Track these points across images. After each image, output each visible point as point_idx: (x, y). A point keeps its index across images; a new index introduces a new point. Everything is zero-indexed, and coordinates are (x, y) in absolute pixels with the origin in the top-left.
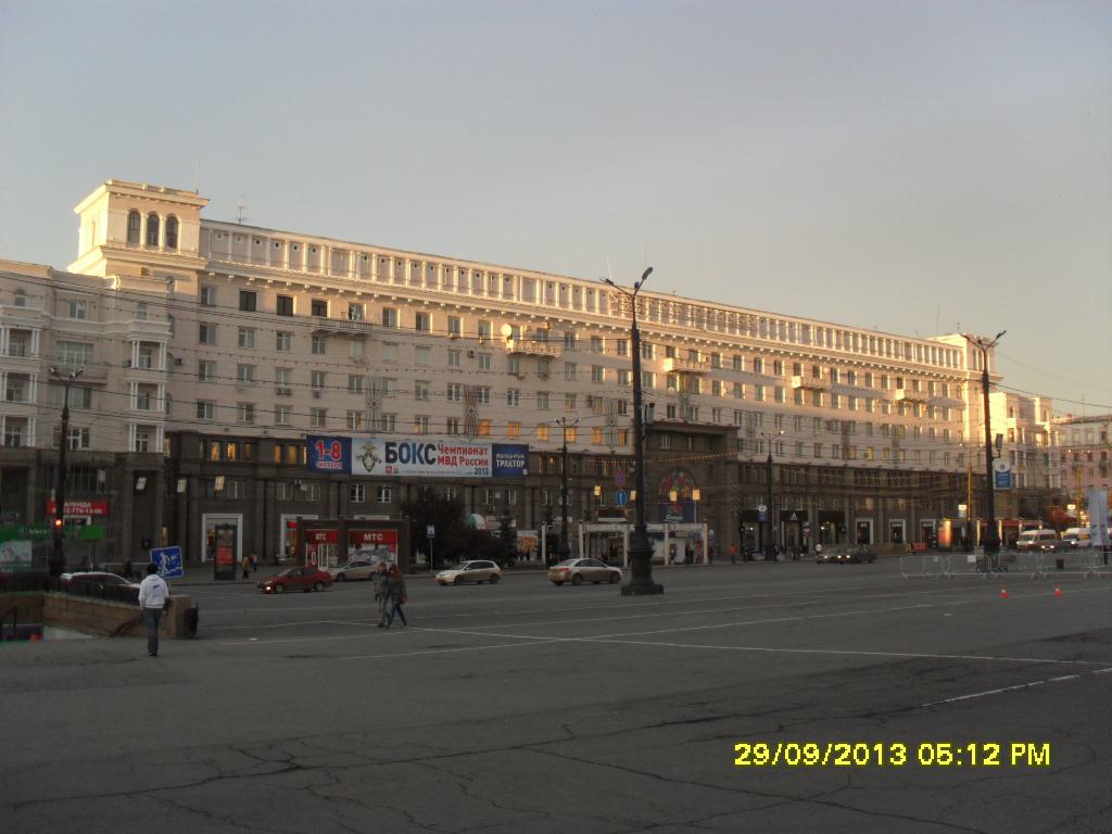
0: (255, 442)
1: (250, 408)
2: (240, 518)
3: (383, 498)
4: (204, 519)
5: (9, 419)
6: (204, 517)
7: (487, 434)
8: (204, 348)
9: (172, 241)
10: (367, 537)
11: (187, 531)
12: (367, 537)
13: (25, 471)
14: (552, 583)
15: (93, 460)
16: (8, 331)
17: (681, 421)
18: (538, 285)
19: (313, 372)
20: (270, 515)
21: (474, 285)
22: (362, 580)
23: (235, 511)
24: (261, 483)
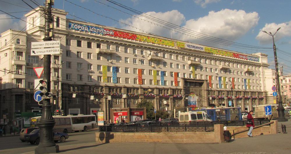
0: (83, 86)
1: (81, 76)
2: (79, 109)
3: (118, 104)
4: (77, 109)
5: (125, 57)
6: (69, 109)
7: (54, 97)
8: (68, 58)
10: (135, 113)
11: (157, 104)
12: (135, 113)
13: (22, 95)
14: (21, 141)
16: (16, 52)
17: (193, 79)
18: (60, 57)
19: (98, 65)
20: (88, 108)
21: (30, 60)
22: (77, 131)
23: (78, 108)
24: (85, 99)
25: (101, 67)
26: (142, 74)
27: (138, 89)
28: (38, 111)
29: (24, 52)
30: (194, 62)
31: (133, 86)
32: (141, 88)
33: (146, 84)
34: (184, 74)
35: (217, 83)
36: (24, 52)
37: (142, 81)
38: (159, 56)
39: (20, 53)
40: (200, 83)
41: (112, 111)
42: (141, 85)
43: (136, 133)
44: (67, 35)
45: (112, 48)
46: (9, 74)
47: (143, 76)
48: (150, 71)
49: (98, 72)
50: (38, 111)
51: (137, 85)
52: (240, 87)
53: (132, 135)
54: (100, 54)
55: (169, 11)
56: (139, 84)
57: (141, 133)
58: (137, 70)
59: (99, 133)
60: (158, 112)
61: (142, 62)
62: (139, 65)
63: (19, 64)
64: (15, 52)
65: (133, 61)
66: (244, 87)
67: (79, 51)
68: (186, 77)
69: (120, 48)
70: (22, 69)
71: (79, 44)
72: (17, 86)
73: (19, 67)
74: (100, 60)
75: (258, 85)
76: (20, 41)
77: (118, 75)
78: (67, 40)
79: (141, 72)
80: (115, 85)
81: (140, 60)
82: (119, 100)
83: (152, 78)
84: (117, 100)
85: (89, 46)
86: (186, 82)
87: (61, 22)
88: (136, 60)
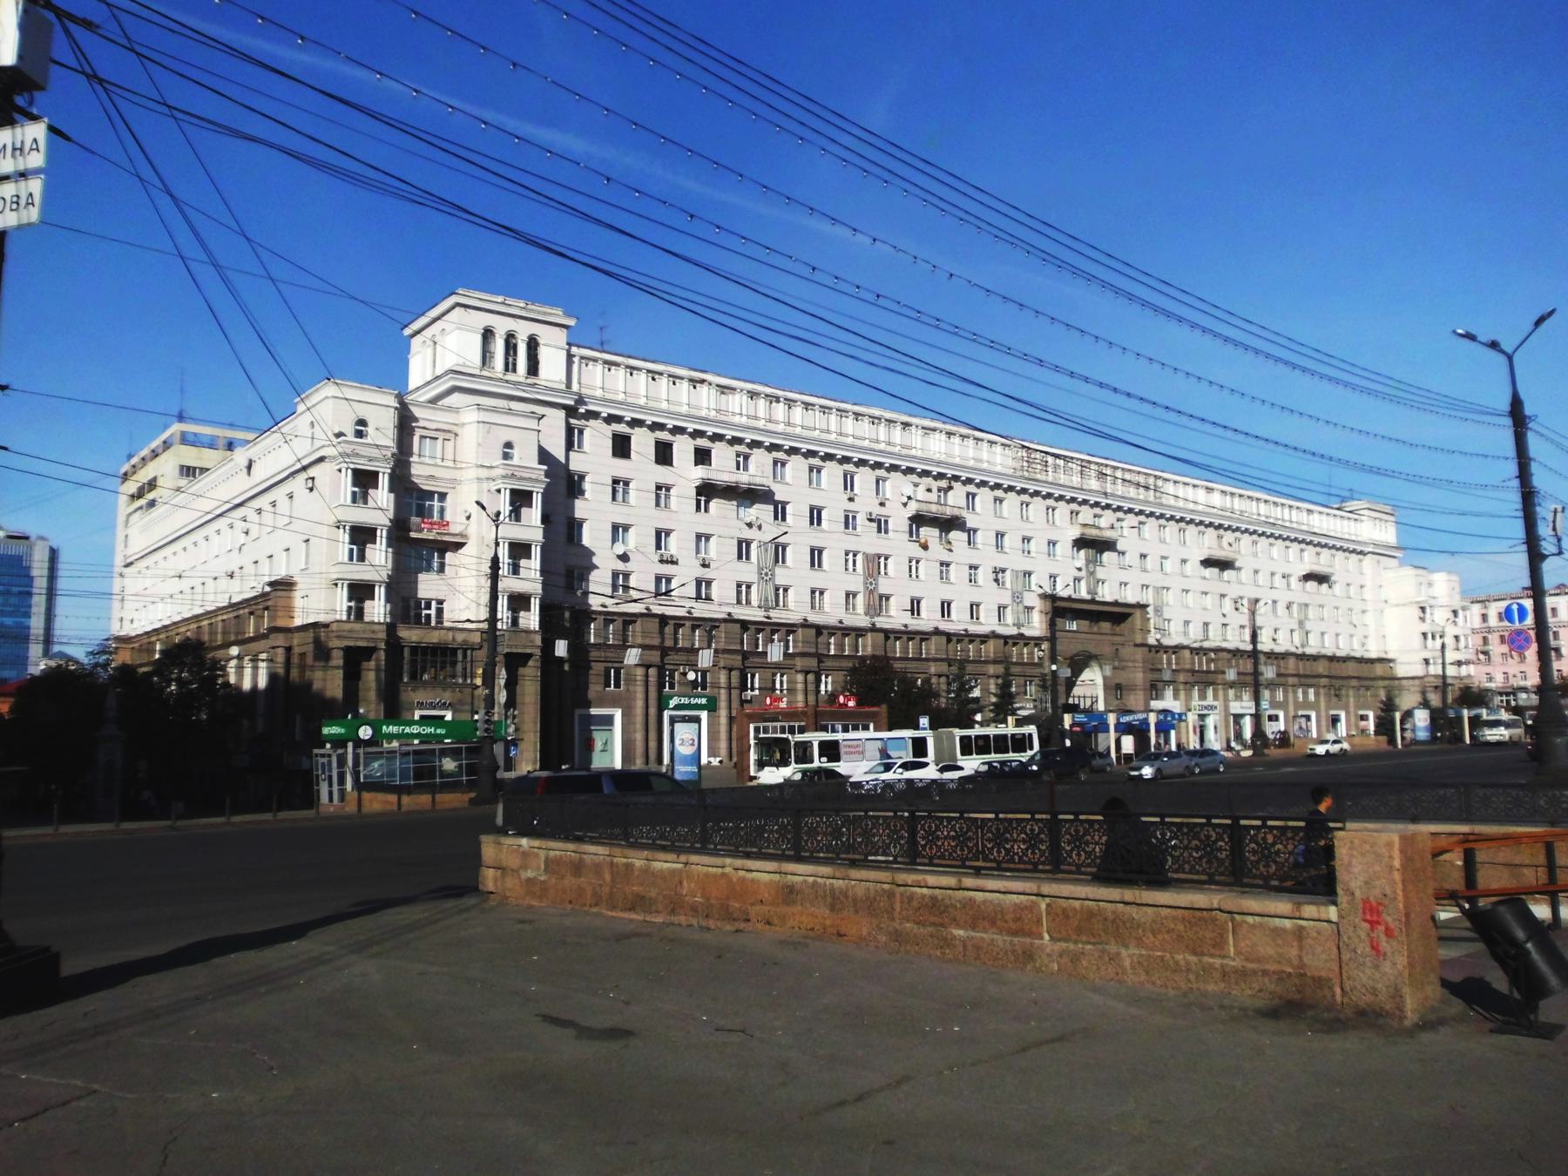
9: (533, 369)
15: (454, 639)
17: (1088, 597)
25: (752, 545)
26: (777, 561)
27: (859, 632)
28: (443, 717)
29: (384, 473)
30: (1093, 533)
31: (966, 630)
32: (874, 629)
33: (896, 617)
34: (1053, 577)
35: (852, 588)
36: (384, 473)
37: (879, 602)
38: (950, 502)
39: (364, 480)
40: (1118, 615)
41: (745, 720)
42: (872, 617)
43: (694, 858)
44: (571, 411)
45: (759, 470)
46: (605, 584)
47: (778, 570)
48: (914, 562)
49: (657, 558)
50: (443, 717)
51: (860, 619)
52: (1278, 636)
53: (673, 872)
54: (707, 491)
55: (1541, 665)
56: (866, 614)
57: (728, 861)
58: (859, 558)
59: (1408, 665)
60: (497, 803)
61: (881, 525)
62: (867, 540)
63: (362, 520)
64: (503, 491)
65: (843, 520)
66: (1296, 635)
67: (661, 480)
68: (1062, 591)
69: (796, 466)
70: (529, 557)
71: (621, 447)
72: (594, 616)
73: (520, 550)
74: (783, 523)
75: (1353, 631)
76: (370, 430)
77: (884, 587)
78: (570, 430)
79: (875, 563)
80: (768, 618)
81: (873, 517)
82: (782, 676)
83: (1006, 598)
84: (774, 675)
85: (664, 454)
86: (1059, 608)
87: (544, 354)
88: (854, 518)
